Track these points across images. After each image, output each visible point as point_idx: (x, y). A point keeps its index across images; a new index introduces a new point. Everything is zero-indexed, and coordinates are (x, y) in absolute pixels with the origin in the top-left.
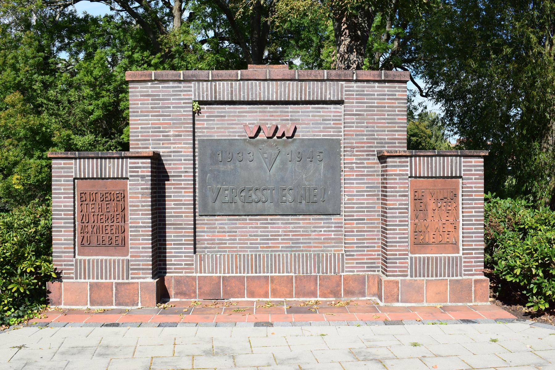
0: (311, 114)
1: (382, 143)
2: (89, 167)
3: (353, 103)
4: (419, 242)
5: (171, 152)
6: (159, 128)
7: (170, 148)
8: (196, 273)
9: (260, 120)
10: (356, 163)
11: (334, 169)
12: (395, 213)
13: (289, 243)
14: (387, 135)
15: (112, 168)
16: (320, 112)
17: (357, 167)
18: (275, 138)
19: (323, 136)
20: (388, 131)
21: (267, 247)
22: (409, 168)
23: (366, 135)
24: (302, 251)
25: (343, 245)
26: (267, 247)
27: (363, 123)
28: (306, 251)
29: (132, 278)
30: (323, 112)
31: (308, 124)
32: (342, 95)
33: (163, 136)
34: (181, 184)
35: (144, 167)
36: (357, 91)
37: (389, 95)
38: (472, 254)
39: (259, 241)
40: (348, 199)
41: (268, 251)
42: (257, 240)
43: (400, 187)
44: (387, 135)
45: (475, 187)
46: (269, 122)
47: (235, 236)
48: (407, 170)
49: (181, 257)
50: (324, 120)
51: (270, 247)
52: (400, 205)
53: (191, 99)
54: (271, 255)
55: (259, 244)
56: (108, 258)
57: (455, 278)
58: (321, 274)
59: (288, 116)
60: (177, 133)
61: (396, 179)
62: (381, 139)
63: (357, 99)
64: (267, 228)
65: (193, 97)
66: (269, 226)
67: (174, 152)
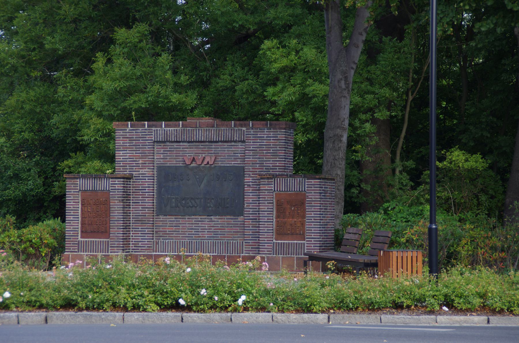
0: (226, 149)
1: (268, 169)
2: (88, 184)
3: (250, 142)
4: (281, 233)
5: (140, 174)
6: (133, 158)
7: (139, 171)
8: (153, 252)
9: (195, 153)
10: (252, 182)
11: (240, 185)
12: (265, 214)
13: (211, 234)
14: (271, 164)
15: (102, 185)
16: (232, 148)
17: (252, 185)
18: (203, 165)
19: (234, 164)
20: (272, 161)
21: (198, 237)
22: (273, 186)
23: (258, 164)
24: (193, 239)
25: (154, 230)
26: (198, 237)
27: (257, 156)
28: (222, 240)
29: (111, 252)
30: (234, 148)
31: (225, 156)
32: (244, 137)
33: (136, 164)
34: (276, 169)
35: (119, 184)
36: (253, 135)
37: (273, 137)
38: (311, 241)
39: (193, 233)
40: (247, 206)
41: (199, 239)
42: (192, 232)
43: (268, 198)
44: (271, 164)
45: (314, 198)
46: (200, 155)
47: (179, 229)
48: (272, 187)
49: (145, 242)
50: (234, 153)
51: (200, 237)
52: (268, 209)
53: (77, 189)
54: (201, 242)
55: (193, 234)
56: (97, 240)
57: (300, 256)
58: (229, 254)
59: (212, 151)
60: (144, 162)
61: (265, 193)
62: (268, 166)
63: (253, 140)
64: (198, 224)
65: (153, 139)
66: (200, 223)
67: (142, 174)
